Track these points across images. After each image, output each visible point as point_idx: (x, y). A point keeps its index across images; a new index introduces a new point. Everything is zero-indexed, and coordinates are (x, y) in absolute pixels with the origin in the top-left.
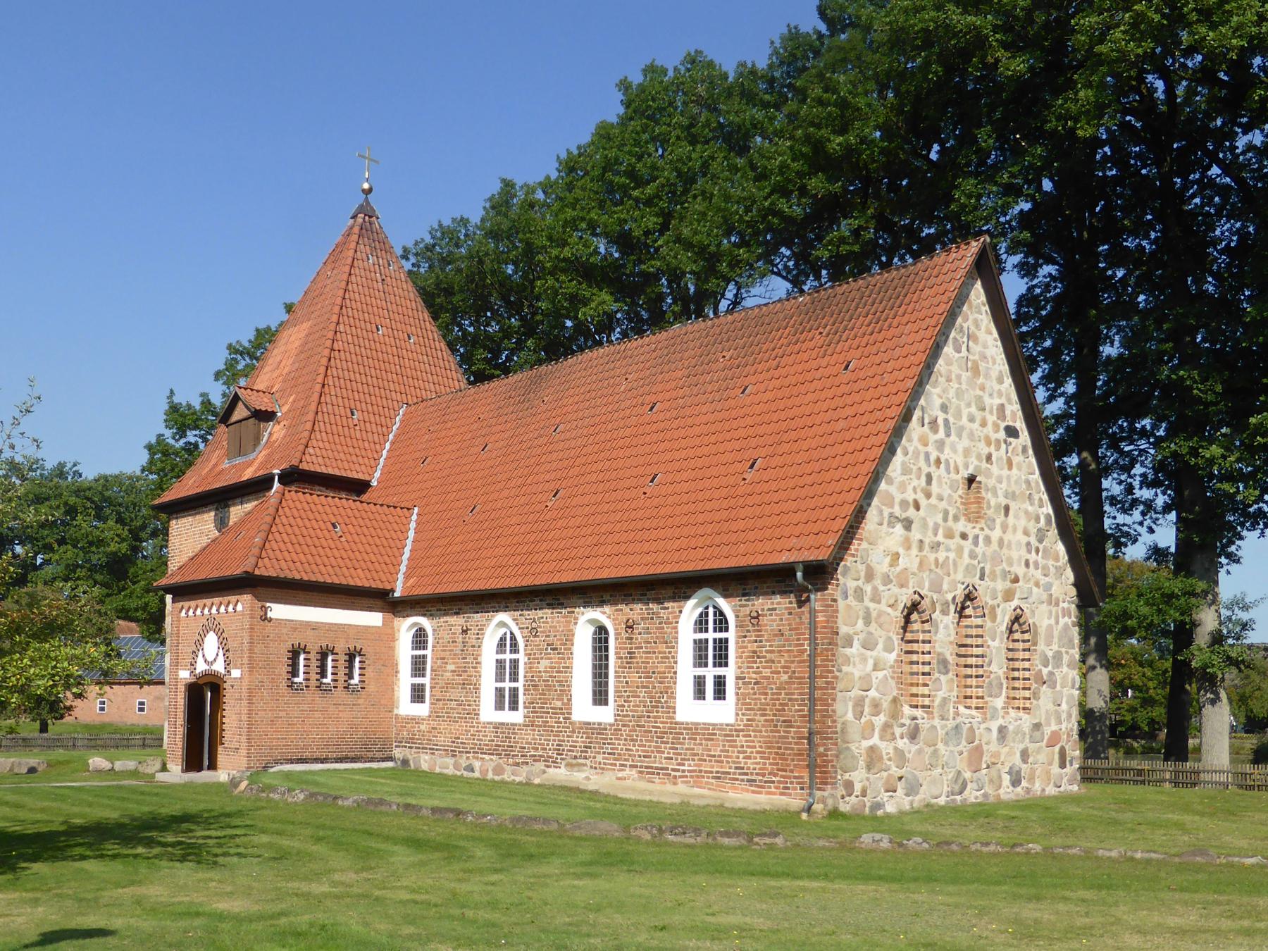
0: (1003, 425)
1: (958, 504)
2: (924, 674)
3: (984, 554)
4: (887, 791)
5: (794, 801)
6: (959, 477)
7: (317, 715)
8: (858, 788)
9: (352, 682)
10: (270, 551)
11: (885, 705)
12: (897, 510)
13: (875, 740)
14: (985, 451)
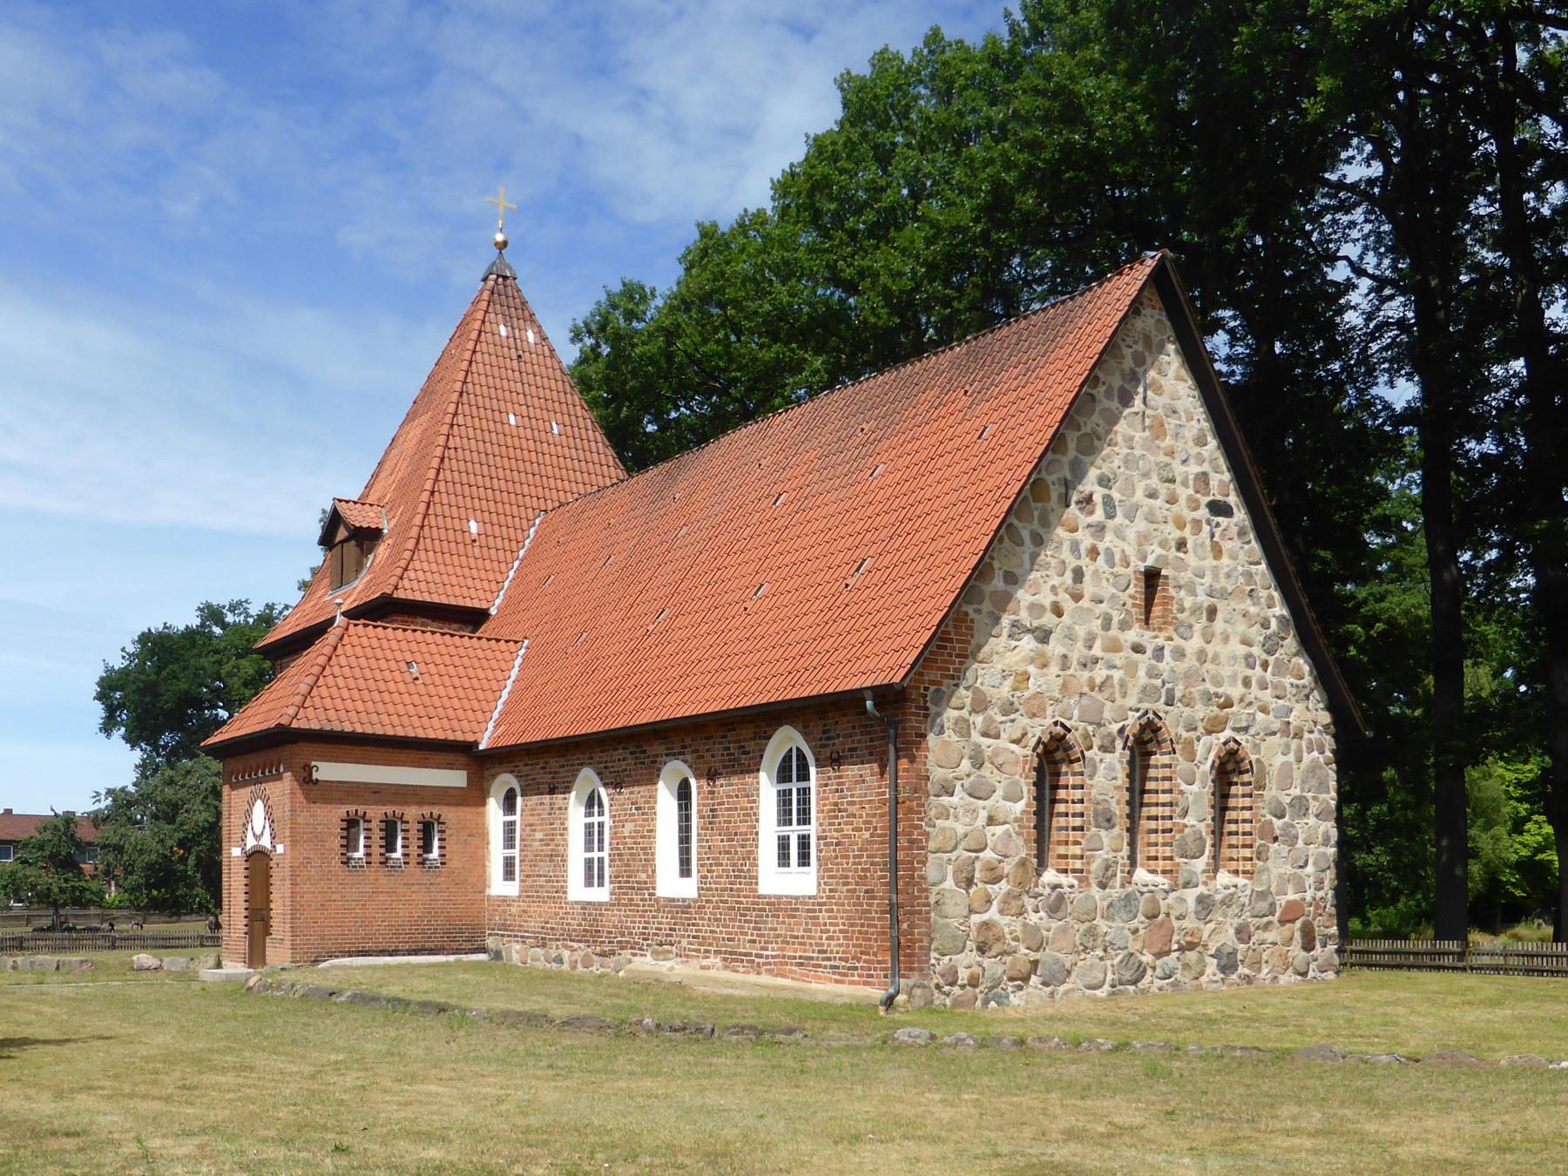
2: (1074, 829)
4: (1011, 979)
6: (1131, 569)
7: (381, 897)
9: (431, 856)
13: (993, 913)
14: (1177, 534)
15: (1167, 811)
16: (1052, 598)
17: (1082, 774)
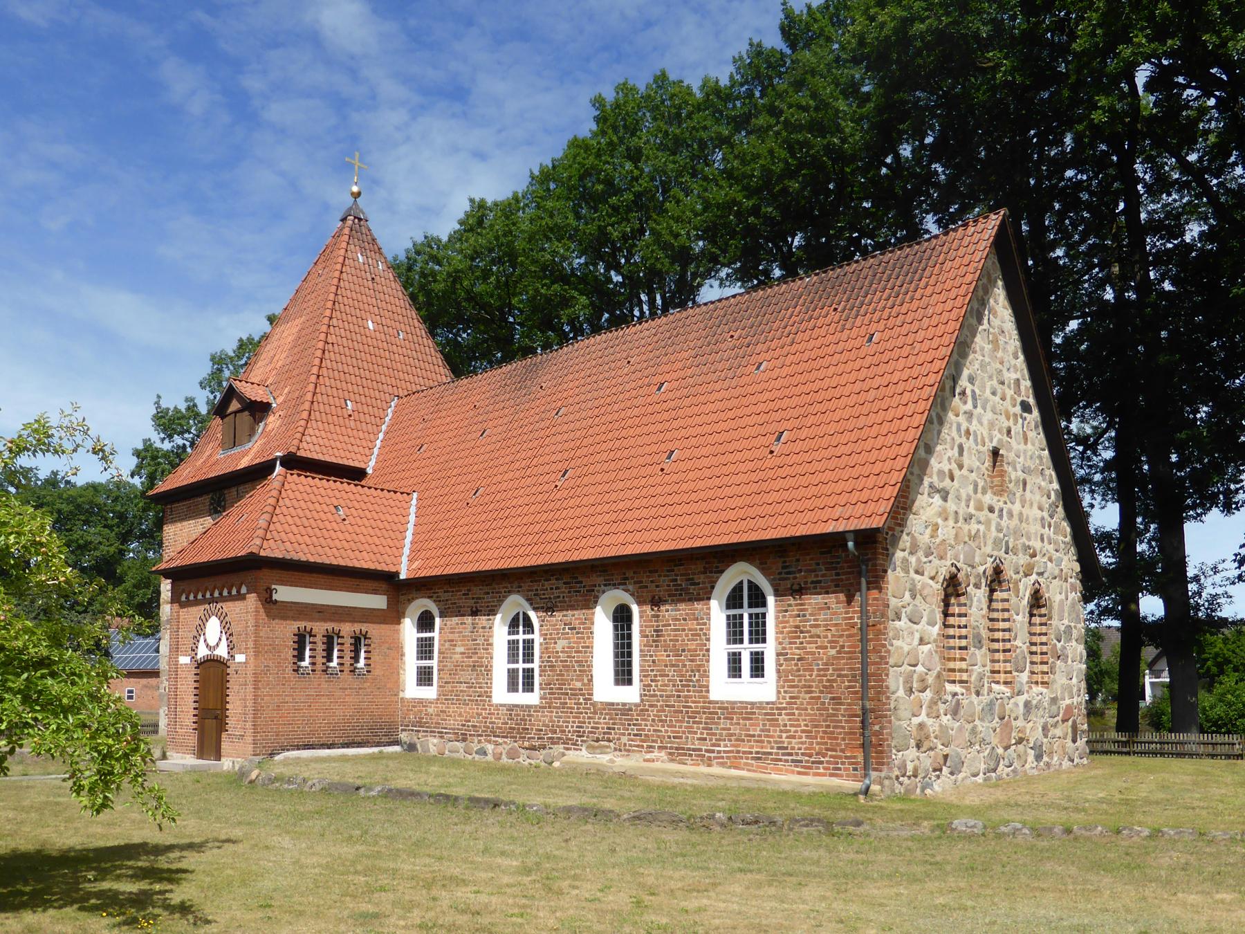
0: (1019, 400)
2: (961, 648)
4: (935, 770)
10: (275, 533)
13: (923, 717)
14: (1006, 424)
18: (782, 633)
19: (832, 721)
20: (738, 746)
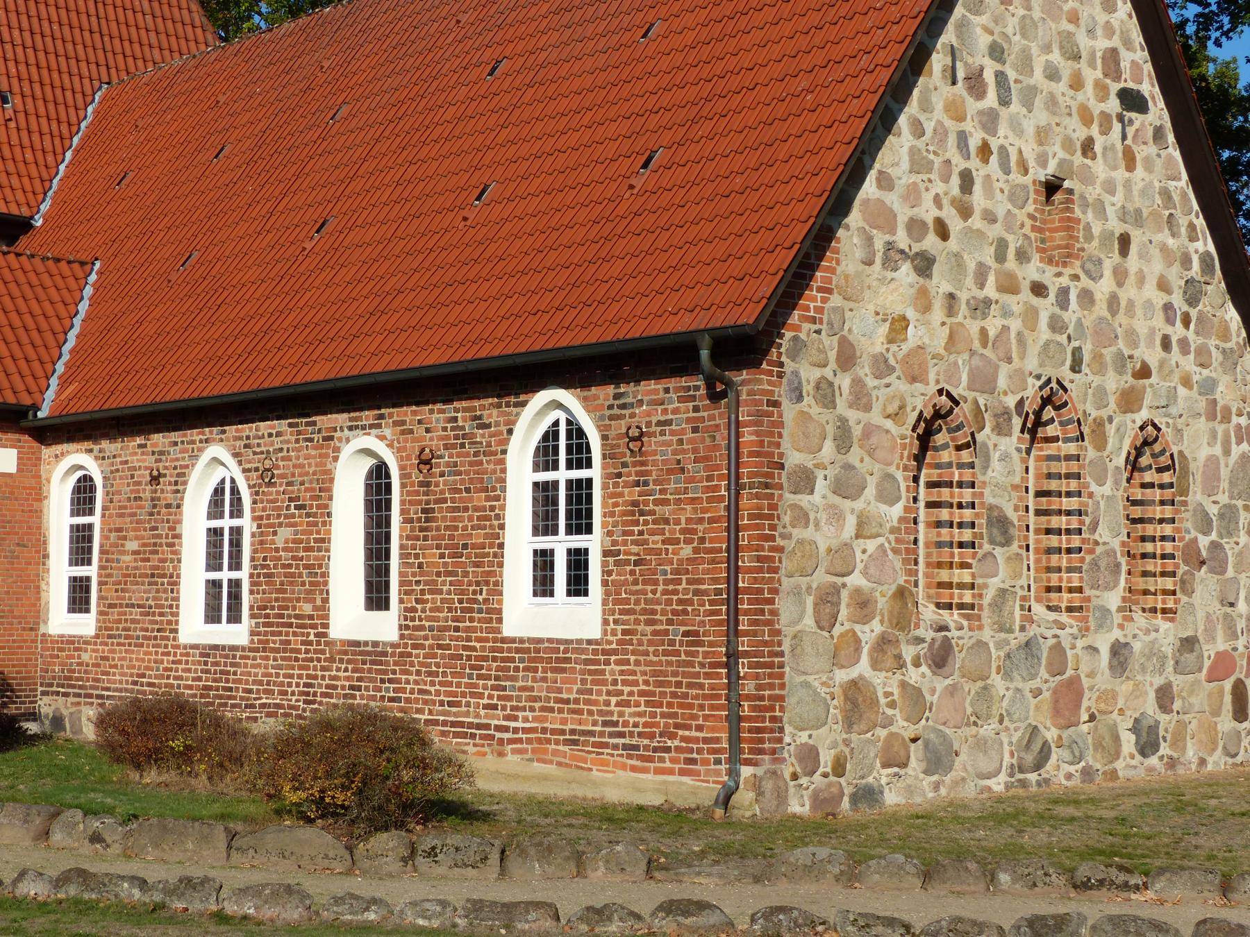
0: (1115, 87)
1: (1027, 230)
2: (961, 545)
3: (1079, 323)
4: (886, 765)
5: (694, 788)
6: (1028, 180)
8: (826, 759)
11: (882, 603)
12: (902, 239)
13: (863, 667)
14: (1081, 133)
15: (1074, 523)
16: (935, 212)
17: (972, 466)
18: (612, 514)
19: (685, 675)
20: (545, 719)
